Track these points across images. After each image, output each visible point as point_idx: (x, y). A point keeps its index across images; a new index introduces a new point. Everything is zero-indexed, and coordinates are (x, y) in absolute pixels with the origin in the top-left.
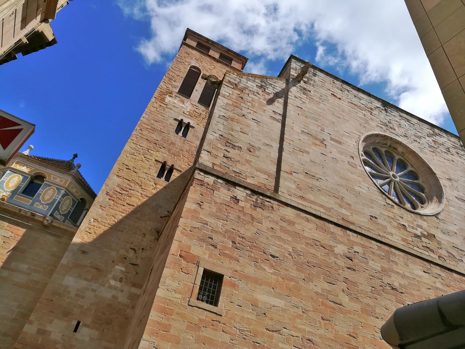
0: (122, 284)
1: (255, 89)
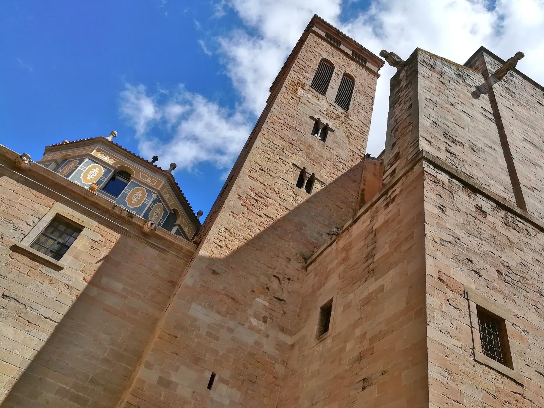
0: (267, 325)
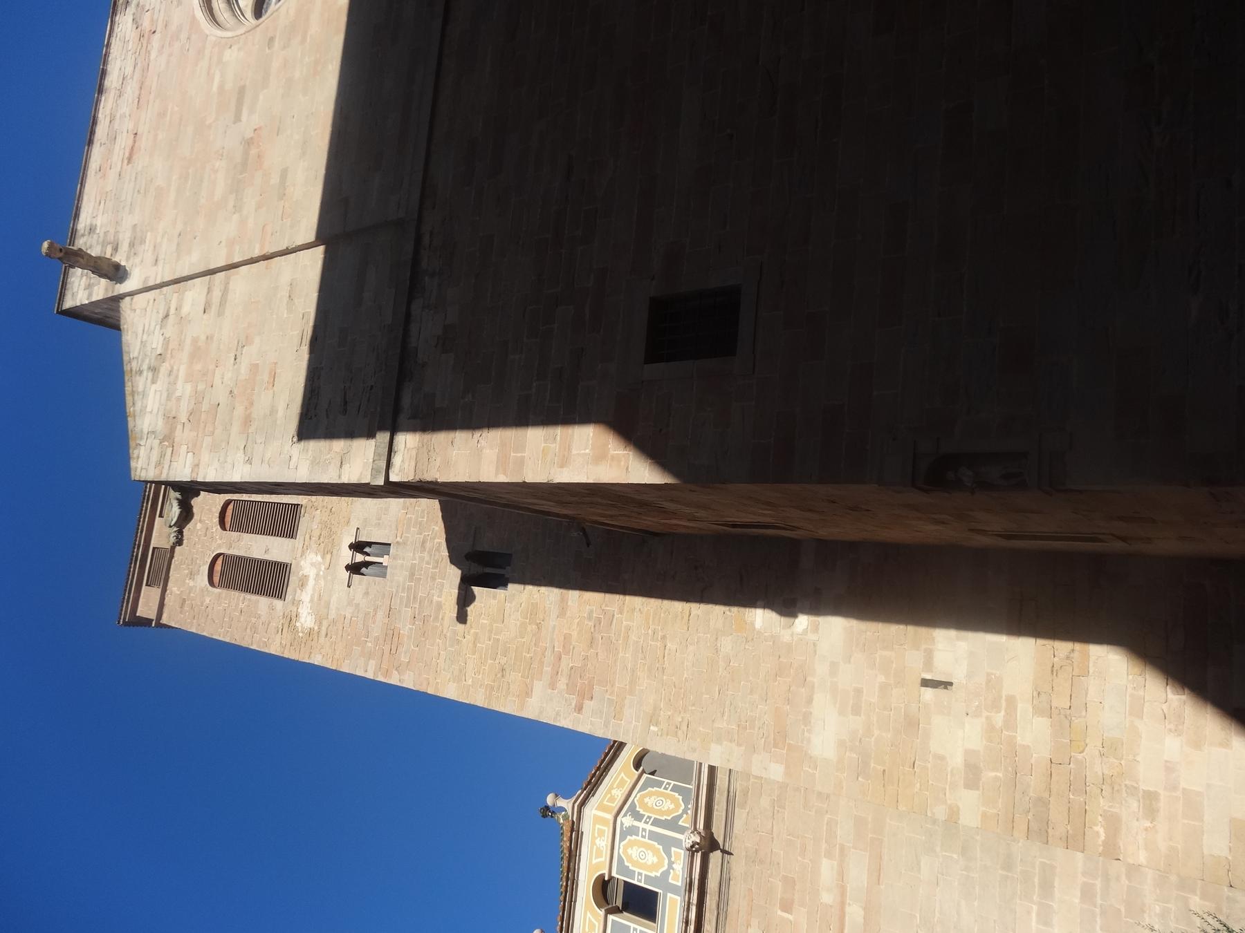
1: (161, 384)
